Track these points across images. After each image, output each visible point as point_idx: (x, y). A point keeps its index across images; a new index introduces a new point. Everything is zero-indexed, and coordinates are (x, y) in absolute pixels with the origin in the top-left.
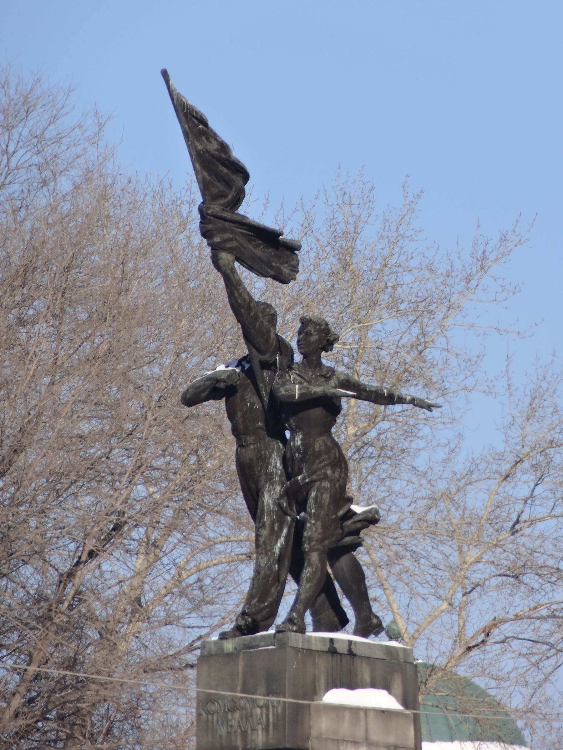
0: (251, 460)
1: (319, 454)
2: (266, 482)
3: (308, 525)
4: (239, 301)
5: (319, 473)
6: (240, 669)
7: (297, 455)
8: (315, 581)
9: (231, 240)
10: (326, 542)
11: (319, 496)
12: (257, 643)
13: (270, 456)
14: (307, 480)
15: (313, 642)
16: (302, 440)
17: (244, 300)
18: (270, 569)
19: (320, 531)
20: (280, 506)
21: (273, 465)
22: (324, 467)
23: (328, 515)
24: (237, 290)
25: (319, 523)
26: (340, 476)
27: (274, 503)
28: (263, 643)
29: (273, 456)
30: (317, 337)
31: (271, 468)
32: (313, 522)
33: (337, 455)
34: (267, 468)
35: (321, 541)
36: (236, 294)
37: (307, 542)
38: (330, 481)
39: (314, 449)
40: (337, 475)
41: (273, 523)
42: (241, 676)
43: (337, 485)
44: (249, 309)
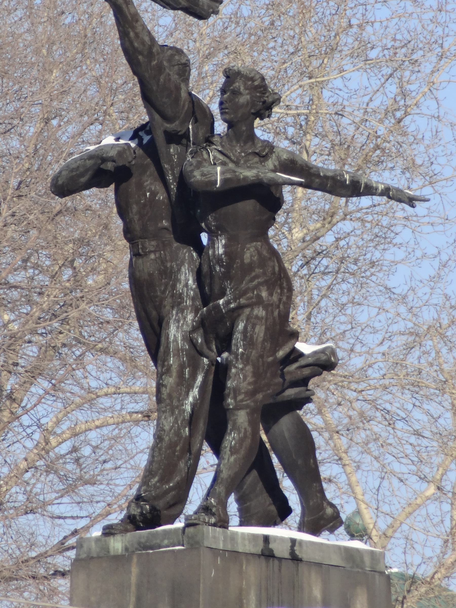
0: (150, 275)
1: (250, 268)
2: (173, 308)
3: (233, 370)
4: (136, 44)
5: (250, 295)
6: (134, 579)
7: (218, 269)
8: (242, 452)
10: (260, 396)
11: (249, 329)
12: (158, 541)
13: (179, 270)
14: (232, 306)
15: (240, 541)
16: (225, 246)
17: (143, 43)
18: (178, 434)
19: (250, 379)
20: (192, 342)
21: (183, 282)
22: (256, 287)
23: (261, 356)
24: (133, 28)
25: (249, 368)
26: (280, 300)
27: (184, 339)
28: (166, 542)
29: (183, 269)
30: (248, 97)
31: (180, 287)
32: (241, 366)
33: (277, 269)
34: (174, 287)
35: (252, 394)
36: (132, 34)
37: (232, 395)
38: (266, 308)
39: (242, 260)
40: (275, 298)
42: (133, 588)
43: (276, 313)
44: (150, 55)
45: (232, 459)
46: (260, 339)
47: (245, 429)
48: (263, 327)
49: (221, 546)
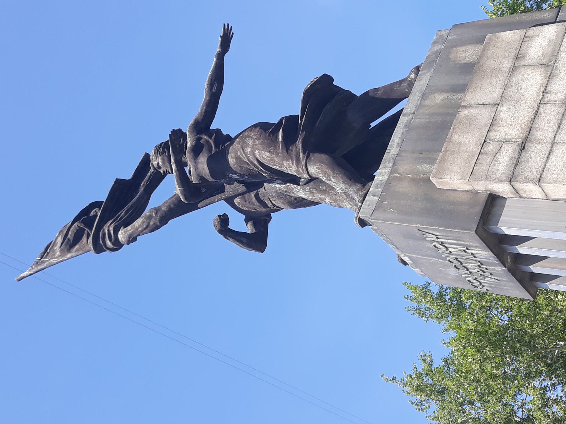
8: (329, 172)
9: (109, 231)
36: (140, 229)
41: (320, 191)
43: (257, 142)
45: (333, 180)
46: (269, 155)
47: (317, 168)
48: (263, 152)
49: (376, 198)
